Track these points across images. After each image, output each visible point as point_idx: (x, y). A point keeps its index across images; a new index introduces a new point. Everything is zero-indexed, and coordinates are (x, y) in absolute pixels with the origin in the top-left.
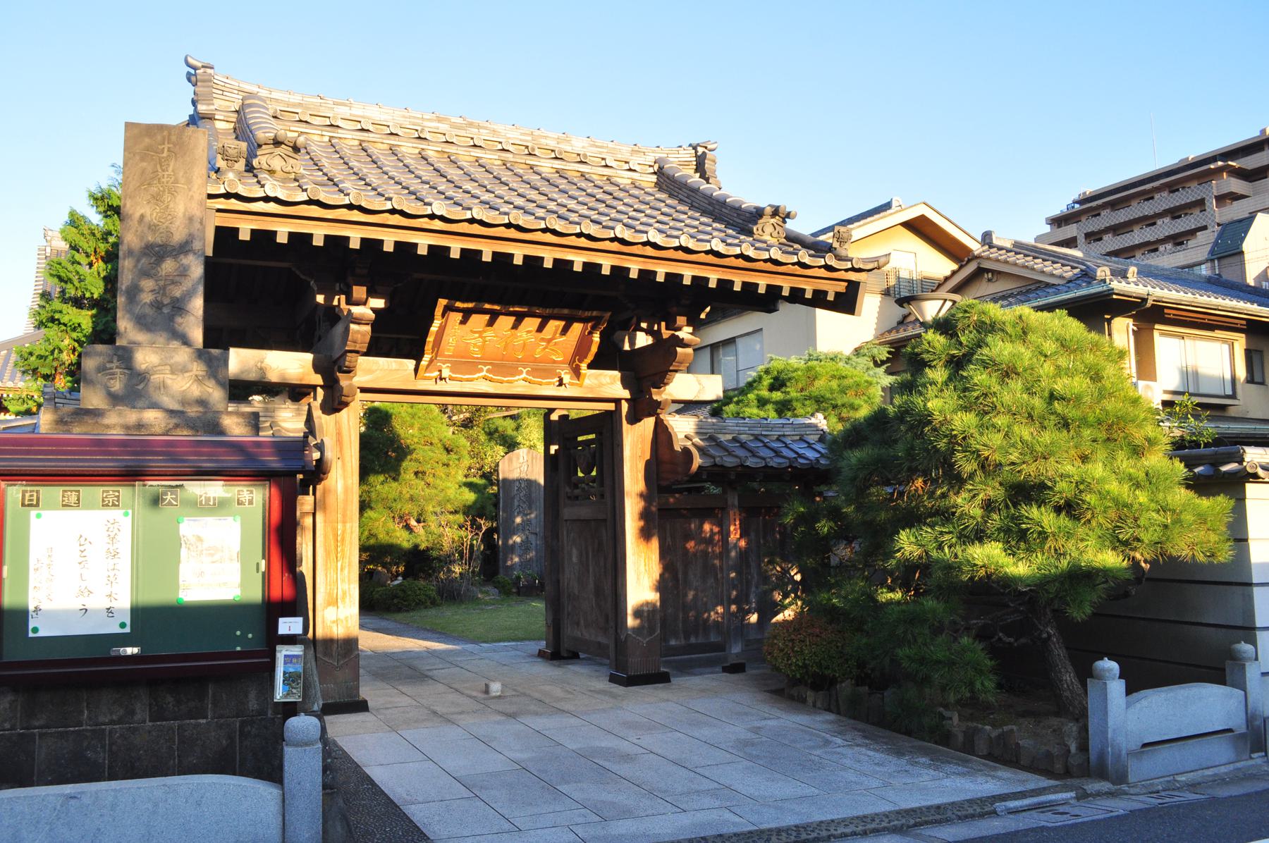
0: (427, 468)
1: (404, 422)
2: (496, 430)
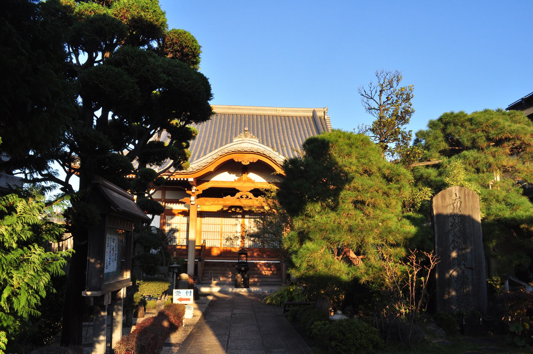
0: (367, 197)
1: (341, 151)
2: (422, 176)
